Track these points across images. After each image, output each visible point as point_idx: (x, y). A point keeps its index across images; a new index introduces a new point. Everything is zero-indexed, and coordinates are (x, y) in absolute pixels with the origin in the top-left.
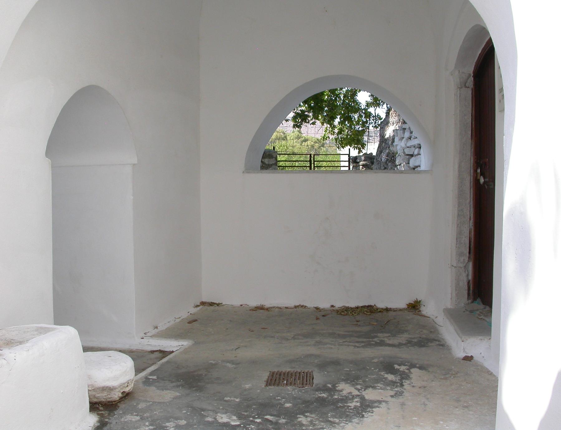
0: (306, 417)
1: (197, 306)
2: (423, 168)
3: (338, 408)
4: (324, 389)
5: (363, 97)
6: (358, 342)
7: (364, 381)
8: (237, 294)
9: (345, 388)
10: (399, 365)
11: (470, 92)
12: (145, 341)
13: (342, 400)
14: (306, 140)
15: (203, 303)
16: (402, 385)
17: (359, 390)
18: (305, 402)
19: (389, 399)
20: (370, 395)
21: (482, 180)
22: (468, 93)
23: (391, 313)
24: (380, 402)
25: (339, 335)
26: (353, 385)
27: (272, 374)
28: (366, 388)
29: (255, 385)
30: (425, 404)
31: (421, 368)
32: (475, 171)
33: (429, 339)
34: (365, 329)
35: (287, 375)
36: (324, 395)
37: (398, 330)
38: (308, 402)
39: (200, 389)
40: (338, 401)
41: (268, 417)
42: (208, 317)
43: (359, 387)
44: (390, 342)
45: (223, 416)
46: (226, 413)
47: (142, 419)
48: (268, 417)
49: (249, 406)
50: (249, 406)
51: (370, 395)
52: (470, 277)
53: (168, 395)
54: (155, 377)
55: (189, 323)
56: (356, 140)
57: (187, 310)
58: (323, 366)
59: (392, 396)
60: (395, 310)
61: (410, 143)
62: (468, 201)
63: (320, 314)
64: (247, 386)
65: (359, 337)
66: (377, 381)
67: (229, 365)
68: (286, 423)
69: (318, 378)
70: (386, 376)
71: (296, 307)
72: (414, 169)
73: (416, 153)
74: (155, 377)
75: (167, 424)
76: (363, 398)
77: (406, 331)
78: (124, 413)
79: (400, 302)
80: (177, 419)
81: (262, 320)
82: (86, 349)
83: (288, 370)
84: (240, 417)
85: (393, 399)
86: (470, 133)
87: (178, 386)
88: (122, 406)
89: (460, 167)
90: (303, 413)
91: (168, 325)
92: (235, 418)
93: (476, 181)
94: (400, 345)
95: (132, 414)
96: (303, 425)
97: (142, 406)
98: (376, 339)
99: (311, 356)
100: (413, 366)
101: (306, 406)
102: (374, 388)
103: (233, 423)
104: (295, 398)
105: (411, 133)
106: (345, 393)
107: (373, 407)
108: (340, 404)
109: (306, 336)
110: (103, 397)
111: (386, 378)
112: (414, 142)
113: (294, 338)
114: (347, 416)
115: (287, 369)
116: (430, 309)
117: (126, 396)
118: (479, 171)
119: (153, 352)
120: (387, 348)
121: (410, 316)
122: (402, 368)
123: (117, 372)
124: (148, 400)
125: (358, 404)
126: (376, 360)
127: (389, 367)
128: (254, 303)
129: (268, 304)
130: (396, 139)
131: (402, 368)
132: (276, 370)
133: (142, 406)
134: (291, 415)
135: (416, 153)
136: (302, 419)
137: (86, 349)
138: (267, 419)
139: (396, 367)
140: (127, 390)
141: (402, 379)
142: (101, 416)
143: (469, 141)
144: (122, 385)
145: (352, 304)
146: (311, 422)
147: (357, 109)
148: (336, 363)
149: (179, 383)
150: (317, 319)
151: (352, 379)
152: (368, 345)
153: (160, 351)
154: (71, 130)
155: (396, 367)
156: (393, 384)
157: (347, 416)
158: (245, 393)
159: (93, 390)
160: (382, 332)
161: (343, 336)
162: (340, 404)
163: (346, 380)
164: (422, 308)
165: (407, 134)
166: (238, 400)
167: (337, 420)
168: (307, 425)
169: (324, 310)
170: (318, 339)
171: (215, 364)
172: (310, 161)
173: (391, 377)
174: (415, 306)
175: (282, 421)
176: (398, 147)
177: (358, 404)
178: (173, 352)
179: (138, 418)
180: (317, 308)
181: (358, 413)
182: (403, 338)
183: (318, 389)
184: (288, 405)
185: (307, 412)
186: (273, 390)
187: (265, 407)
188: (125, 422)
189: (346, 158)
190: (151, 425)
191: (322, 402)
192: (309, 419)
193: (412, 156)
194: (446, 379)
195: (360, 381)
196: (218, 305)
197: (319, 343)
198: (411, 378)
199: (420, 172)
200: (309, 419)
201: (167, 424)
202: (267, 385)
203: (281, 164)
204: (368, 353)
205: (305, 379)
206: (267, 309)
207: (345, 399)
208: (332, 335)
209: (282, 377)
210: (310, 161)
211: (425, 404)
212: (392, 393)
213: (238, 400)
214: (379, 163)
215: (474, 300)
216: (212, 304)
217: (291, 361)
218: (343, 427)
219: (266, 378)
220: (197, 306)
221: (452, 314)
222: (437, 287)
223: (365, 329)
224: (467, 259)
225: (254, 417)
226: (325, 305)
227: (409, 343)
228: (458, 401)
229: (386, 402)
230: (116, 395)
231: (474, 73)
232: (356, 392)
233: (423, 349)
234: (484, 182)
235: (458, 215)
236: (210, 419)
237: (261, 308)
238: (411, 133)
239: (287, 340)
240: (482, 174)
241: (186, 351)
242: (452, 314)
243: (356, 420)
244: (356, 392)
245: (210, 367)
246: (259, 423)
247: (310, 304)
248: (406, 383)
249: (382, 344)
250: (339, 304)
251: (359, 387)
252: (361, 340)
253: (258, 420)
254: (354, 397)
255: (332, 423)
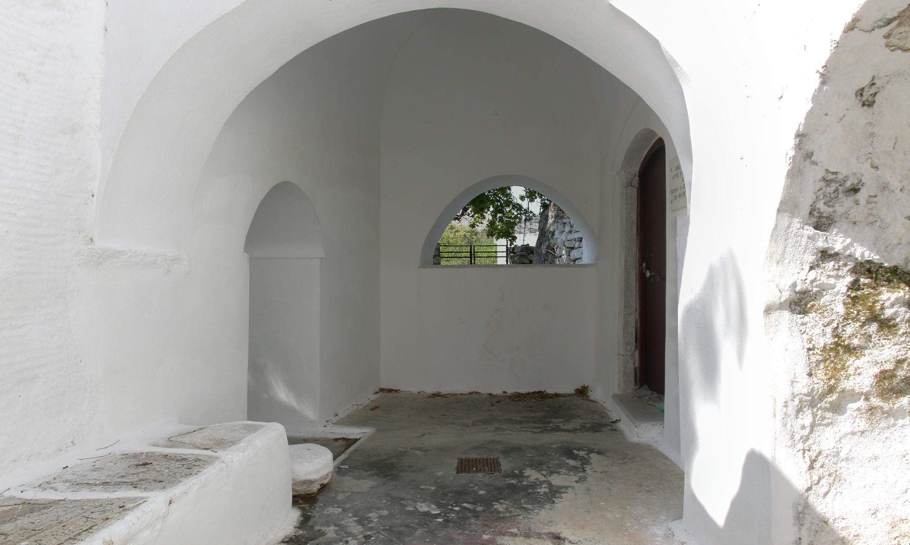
0: (501, 504)
1: (377, 393)
2: (586, 260)
3: (529, 494)
4: (512, 475)
5: (517, 192)
6: (534, 428)
7: (548, 467)
8: (415, 383)
9: (532, 475)
10: (578, 450)
11: (635, 191)
12: (328, 429)
13: (531, 486)
14: (457, 231)
15: (382, 390)
16: (584, 471)
17: (545, 476)
18: (497, 489)
19: (574, 484)
20: (556, 480)
21: (648, 274)
22: (634, 192)
23: (560, 399)
24: (567, 487)
25: (516, 421)
26: (538, 471)
27: (461, 461)
28: (551, 473)
29: (447, 472)
30: (610, 490)
31: (599, 453)
32: (641, 265)
33: (601, 424)
34: (539, 414)
35: (475, 462)
36: (514, 481)
37: (569, 418)
38: (500, 488)
39: (395, 478)
40: (528, 487)
41: (465, 505)
42: (386, 405)
43: (544, 472)
44: (565, 427)
45: (423, 505)
46: (424, 502)
47: (344, 510)
48: (465, 505)
49: (445, 494)
50: (445, 494)
51: (556, 480)
52: (637, 365)
53: (366, 484)
54: (347, 467)
55: (372, 409)
56: (508, 233)
57: (367, 398)
58: (509, 451)
59: (577, 482)
60: (564, 396)
61: (570, 237)
62: (634, 293)
63: (494, 400)
64: (440, 474)
65: (534, 423)
66: (561, 466)
67: (418, 452)
68: (484, 511)
69: (505, 465)
70: (567, 461)
71: (470, 393)
72: (575, 261)
73: (577, 246)
74: (347, 467)
75: (370, 515)
76: (550, 485)
77: (579, 416)
78: (324, 505)
79: (568, 388)
80: (378, 509)
81: (441, 407)
82: (292, 441)
83: (476, 456)
84: (439, 506)
85: (578, 485)
86: (635, 229)
87: (373, 475)
88: (321, 498)
89: (626, 261)
90: (497, 501)
91: (347, 413)
92: (434, 506)
93: (642, 275)
94: (574, 430)
95: (333, 507)
96: (500, 512)
97: (340, 497)
98: (551, 425)
99: (493, 442)
100: (591, 451)
101: (499, 493)
102: (558, 473)
103: (433, 512)
104: (487, 485)
105: (572, 227)
106: (532, 479)
107: (561, 493)
108: (530, 491)
109: (485, 422)
110: (302, 490)
111: (568, 464)
112: (576, 236)
113: (473, 424)
114: (539, 502)
115: (474, 456)
116: (597, 394)
117: (323, 487)
118: (644, 265)
119: (336, 440)
120: (563, 433)
121: (579, 401)
122: (581, 453)
123: (318, 464)
124: (346, 490)
125: (547, 490)
126: (555, 446)
127: (568, 452)
128: (431, 390)
129: (444, 391)
130: (557, 233)
131: (581, 453)
132: (463, 457)
133: (340, 497)
134: (487, 502)
135: (577, 246)
136: (497, 506)
137: (292, 441)
138: (465, 507)
139: (575, 452)
140: (325, 482)
141: (583, 464)
142: (303, 509)
143: (635, 237)
144: (323, 478)
145: (523, 390)
146: (507, 509)
147: (509, 203)
148: (518, 449)
149: (373, 472)
150: (493, 405)
151: (537, 465)
152: (545, 430)
153: (344, 439)
154: (270, 222)
155: (575, 452)
156: (574, 469)
157: (539, 502)
158: (439, 481)
159: (295, 484)
160: (555, 418)
161: (520, 422)
162: (530, 491)
163: (531, 466)
164: (590, 394)
165: (567, 229)
166: (433, 488)
167: (530, 507)
168: (503, 513)
169: (497, 396)
170: (496, 425)
171: (405, 452)
172: (471, 252)
173: (572, 462)
174: (582, 392)
175: (480, 508)
176: (559, 240)
177: (547, 490)
178: (356, 440)
179: (340, 510)
180: (490, 395)
181: (550, 500)
182: (577, 423)
183: (507, 476)
184: (482, 492)
185: (501, 499)
186: (464, 478)
187: (461, 494)
188: (329, 515)
189: (504, 249)
190: (355, 516)
191: (512, 487)
192: (504, 506)
193: (573, 248)
194: (624, 463)
195: (544, 467)
196: (396, 391)
197: (499, 429)
198: (591, 464)
199: (581, 266)
200: (504, 506)
201: (370, 515)
202: (458, 472)
203: (446, 255)
204: (546, 439)
205: (492, 466)
206: (444, 396)
207: (534, 485)
208: (509, 421)
209: (471, 464)
210: (471, 252)
211: (610, 490)
212: (577, 479)
213: (433, 488)
214: (540, 254)
215: (641, 386)
216: (390, 391)
217: (476, 448)
218: (537, 514)
219: (455, 465)
220: (377, 393)
221: (621, 399)
222: (604, 372)
223: (539, 414)
224: (633, 348)
225: (452, 505)
226: (497, 391)
227: (583, 428)
228: (640, 485)
229: (572, 487)
230: (315, 488)
231: (639, 172)
232: (542, 479)
233: (598, 434)
234: (651, 276)
235: (625, 307)
236: (410, 509)
237: (437, 395)
238: (572, 227)
239: (468, 426)
240: (648, 268)
241: (371, 439)
242: (621, 399)
243: (548, 506)
244: (542, 479)
245: (401, 455)
246: (458, 512)
247: (484, 390)
248: (588, 468)
249: (557, 429)
250: (510, 391)
251: (544, 472)
252: (537, 425)
253: (457, 509)
254: (541, 483)
255: (527, 510)
